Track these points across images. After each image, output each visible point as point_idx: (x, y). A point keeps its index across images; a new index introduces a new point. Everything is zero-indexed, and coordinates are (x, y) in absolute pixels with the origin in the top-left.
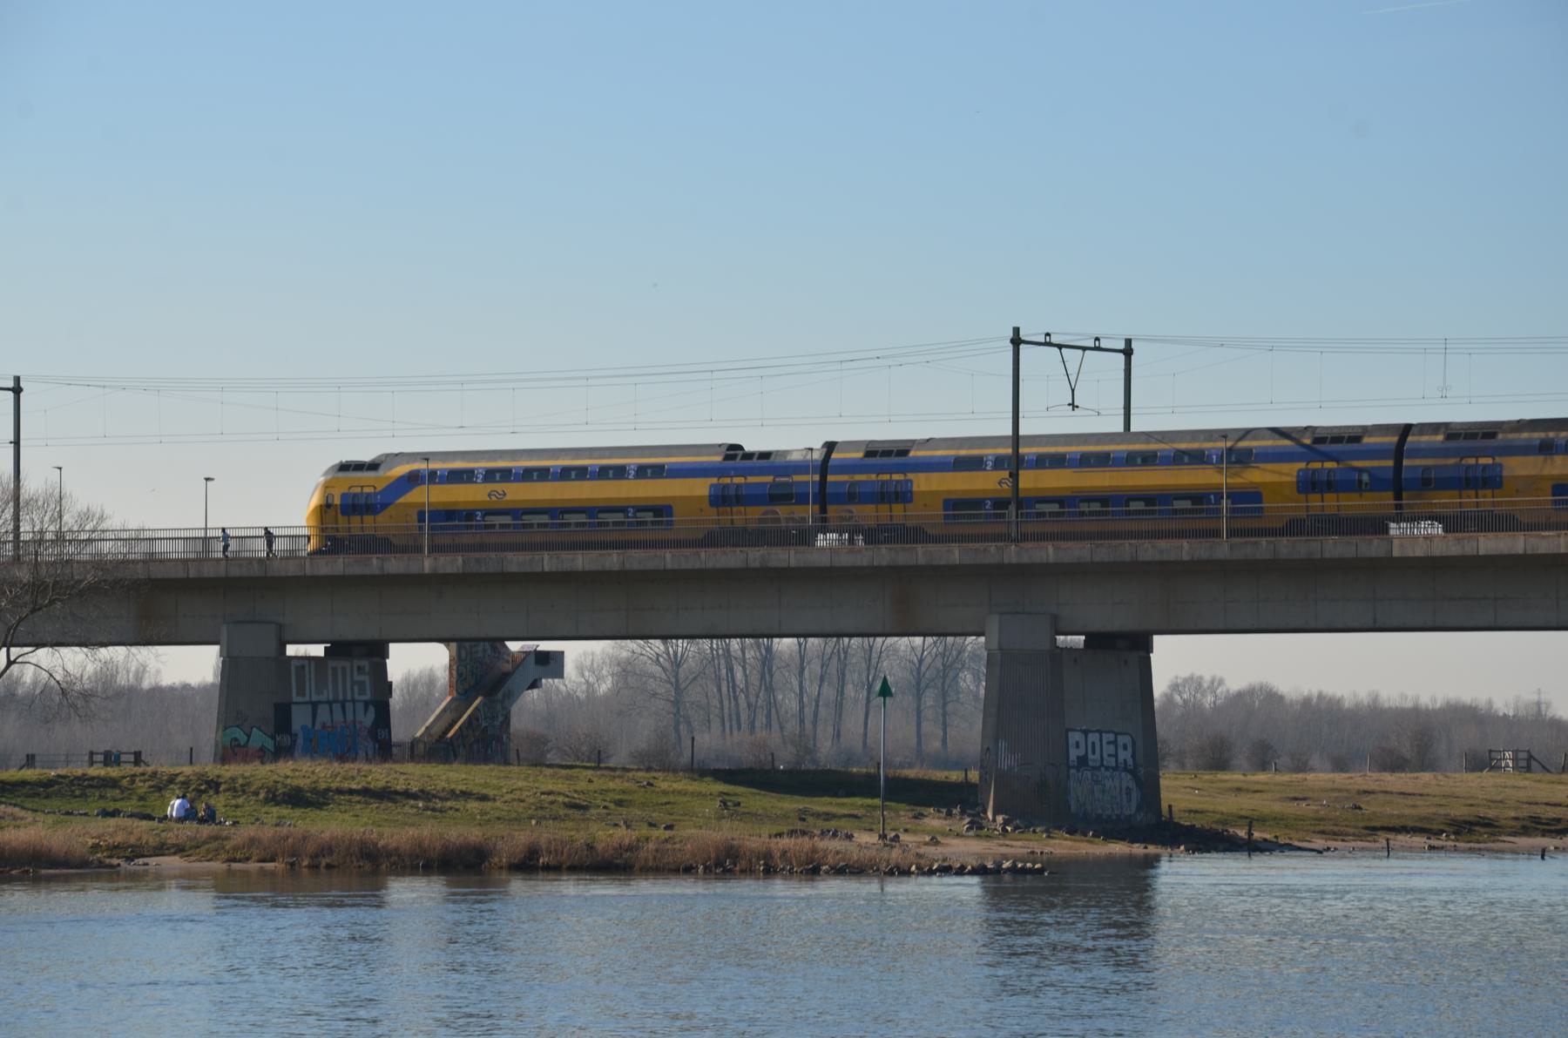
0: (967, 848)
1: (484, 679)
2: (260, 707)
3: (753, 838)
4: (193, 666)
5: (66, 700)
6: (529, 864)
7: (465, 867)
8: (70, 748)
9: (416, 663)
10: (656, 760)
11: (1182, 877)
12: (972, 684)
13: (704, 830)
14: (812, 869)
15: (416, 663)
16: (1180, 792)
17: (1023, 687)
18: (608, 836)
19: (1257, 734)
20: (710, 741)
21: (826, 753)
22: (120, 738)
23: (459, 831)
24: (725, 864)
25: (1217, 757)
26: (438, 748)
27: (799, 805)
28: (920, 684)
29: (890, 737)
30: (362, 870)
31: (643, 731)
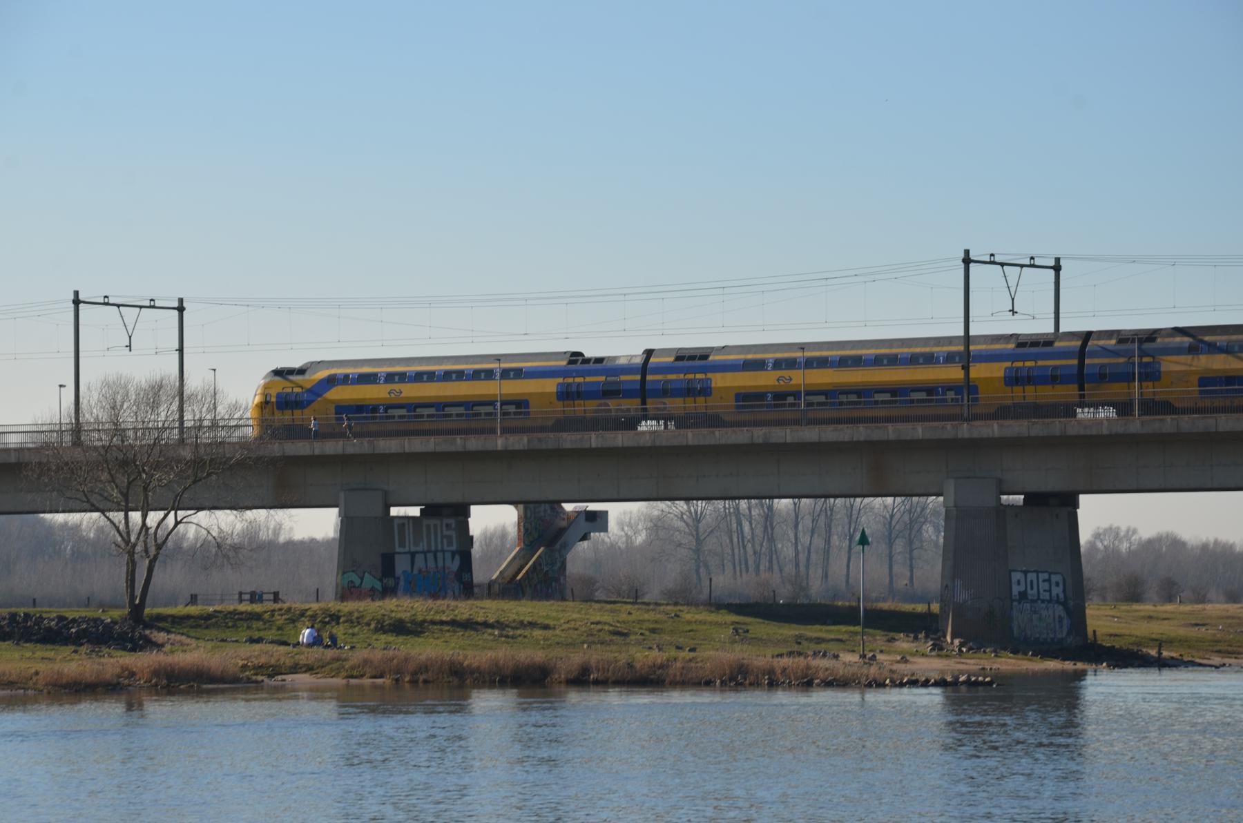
0: (931, 665)
1: (545, 533)
2: (370, 556)
3: (759, 658)
4: (317, 524)
5: (221, 552)
6: (582, 679)
7: (531, 681)
8: (225, 590)
9: (493, 521)
10: (681, 597)
11: (1104, 688)
12: (933, 535)
13: (720, 652)
14: (807, 683)
15: (493, 521)
16: (1102, 620)
17: (975, 539)
18: (644, 657)
19: (1163, 573)
20: (724, 582)
21: (817, 590)
22: (263, 581)
23: (527, 654)
24: (738, 678)
25: (1132, 592)
26: (510, 588)
27: (795, 632)
28: (892, 535)
29: (865, 576)
30: (453, 684)
31: (671, 574)
